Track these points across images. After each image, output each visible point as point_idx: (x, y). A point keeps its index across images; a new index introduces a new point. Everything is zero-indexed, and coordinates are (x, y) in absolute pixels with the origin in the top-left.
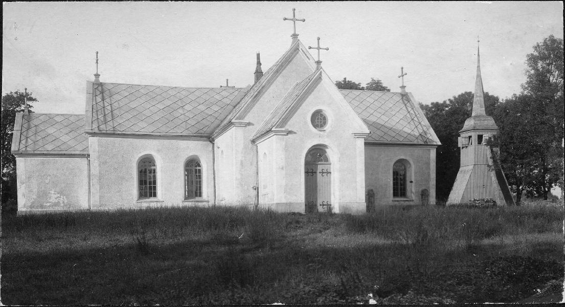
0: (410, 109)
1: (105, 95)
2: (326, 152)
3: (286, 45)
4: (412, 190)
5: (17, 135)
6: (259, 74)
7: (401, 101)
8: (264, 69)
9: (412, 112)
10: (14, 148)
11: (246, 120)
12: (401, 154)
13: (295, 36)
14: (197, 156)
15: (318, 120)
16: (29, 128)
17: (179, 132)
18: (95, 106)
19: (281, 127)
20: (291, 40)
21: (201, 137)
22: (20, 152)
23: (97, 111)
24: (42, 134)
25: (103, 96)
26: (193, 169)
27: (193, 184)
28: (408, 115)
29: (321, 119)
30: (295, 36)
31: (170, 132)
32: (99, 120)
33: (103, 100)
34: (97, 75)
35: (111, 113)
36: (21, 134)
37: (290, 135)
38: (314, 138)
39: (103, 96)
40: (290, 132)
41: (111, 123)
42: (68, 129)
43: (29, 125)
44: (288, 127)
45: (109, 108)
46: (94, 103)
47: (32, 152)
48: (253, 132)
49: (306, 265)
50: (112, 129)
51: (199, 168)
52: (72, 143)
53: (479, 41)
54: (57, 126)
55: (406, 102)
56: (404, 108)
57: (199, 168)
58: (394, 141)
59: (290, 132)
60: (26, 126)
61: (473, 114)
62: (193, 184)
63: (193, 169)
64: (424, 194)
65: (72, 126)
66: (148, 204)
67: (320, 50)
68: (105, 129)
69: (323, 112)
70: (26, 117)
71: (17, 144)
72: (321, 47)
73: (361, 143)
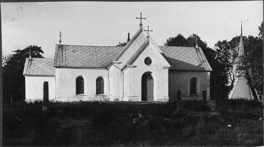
0: (199, 55)
1: (63, 50)
2: (151, 75)
3: (138, 28)
4: (199, 90)
5: (26, 67)
6: (129, 40)
7: (196, 51)
8: (131, 38)
9: (200, 56)
10: (24, 73)
11: (119, 61)
12: (194, 75)
13: (141, 25)
14: (101, 76)
15: (148, 61)
16: (31, 64)
17: (95, 65)
18: (58, 55)
19: (131, 65)
20: (139, 27)
21: (103, 68)
22: (27, 74)
23: (59, 57)
24: (37, 67)
25: (62, 51)
26: (100, 81)
27: (100, 89)
28: (198, 58)
29: (149, 61)
30: (141, 25)
31: (90, 66)
32: (60, 61)
33: (62, 52)
34: (60, 41)
35: (49, 62)
36: (28, 67)
37: (135, 68)
38: (147, 69)
39: (62, 51)
40: (135, 67)
41: (65, 62)
42: (47, 65)
43: (31, 63)
44: (134, 64)
45: (64, 56)
46: (58, 54)
47: (32, 75)
48: (121, 66)
49: (234, 139)
50: (65, 65)
51: (83, 81)
52: (49, 71)
53: (242, 22)
54: (43, 63)
55: (197, 51)
56: (197, 54)
57: (83, 81)
58: (190, 69)
59: (135, 67)
60: (30, 63)
61: (239, 56)
62: (100, 89)
63: (100, 81)
64: (204, 93)
65: (49, 64)
66: (99, 98)
67: (149, 31)
68: (62, 65)
69: (150, 58)
70: (30, 60)
71: (26, 71)
72: (149, 30)
73: (167, 71)
